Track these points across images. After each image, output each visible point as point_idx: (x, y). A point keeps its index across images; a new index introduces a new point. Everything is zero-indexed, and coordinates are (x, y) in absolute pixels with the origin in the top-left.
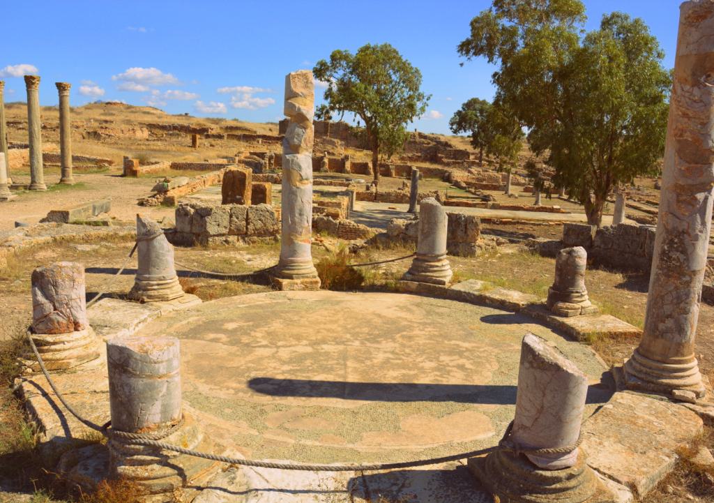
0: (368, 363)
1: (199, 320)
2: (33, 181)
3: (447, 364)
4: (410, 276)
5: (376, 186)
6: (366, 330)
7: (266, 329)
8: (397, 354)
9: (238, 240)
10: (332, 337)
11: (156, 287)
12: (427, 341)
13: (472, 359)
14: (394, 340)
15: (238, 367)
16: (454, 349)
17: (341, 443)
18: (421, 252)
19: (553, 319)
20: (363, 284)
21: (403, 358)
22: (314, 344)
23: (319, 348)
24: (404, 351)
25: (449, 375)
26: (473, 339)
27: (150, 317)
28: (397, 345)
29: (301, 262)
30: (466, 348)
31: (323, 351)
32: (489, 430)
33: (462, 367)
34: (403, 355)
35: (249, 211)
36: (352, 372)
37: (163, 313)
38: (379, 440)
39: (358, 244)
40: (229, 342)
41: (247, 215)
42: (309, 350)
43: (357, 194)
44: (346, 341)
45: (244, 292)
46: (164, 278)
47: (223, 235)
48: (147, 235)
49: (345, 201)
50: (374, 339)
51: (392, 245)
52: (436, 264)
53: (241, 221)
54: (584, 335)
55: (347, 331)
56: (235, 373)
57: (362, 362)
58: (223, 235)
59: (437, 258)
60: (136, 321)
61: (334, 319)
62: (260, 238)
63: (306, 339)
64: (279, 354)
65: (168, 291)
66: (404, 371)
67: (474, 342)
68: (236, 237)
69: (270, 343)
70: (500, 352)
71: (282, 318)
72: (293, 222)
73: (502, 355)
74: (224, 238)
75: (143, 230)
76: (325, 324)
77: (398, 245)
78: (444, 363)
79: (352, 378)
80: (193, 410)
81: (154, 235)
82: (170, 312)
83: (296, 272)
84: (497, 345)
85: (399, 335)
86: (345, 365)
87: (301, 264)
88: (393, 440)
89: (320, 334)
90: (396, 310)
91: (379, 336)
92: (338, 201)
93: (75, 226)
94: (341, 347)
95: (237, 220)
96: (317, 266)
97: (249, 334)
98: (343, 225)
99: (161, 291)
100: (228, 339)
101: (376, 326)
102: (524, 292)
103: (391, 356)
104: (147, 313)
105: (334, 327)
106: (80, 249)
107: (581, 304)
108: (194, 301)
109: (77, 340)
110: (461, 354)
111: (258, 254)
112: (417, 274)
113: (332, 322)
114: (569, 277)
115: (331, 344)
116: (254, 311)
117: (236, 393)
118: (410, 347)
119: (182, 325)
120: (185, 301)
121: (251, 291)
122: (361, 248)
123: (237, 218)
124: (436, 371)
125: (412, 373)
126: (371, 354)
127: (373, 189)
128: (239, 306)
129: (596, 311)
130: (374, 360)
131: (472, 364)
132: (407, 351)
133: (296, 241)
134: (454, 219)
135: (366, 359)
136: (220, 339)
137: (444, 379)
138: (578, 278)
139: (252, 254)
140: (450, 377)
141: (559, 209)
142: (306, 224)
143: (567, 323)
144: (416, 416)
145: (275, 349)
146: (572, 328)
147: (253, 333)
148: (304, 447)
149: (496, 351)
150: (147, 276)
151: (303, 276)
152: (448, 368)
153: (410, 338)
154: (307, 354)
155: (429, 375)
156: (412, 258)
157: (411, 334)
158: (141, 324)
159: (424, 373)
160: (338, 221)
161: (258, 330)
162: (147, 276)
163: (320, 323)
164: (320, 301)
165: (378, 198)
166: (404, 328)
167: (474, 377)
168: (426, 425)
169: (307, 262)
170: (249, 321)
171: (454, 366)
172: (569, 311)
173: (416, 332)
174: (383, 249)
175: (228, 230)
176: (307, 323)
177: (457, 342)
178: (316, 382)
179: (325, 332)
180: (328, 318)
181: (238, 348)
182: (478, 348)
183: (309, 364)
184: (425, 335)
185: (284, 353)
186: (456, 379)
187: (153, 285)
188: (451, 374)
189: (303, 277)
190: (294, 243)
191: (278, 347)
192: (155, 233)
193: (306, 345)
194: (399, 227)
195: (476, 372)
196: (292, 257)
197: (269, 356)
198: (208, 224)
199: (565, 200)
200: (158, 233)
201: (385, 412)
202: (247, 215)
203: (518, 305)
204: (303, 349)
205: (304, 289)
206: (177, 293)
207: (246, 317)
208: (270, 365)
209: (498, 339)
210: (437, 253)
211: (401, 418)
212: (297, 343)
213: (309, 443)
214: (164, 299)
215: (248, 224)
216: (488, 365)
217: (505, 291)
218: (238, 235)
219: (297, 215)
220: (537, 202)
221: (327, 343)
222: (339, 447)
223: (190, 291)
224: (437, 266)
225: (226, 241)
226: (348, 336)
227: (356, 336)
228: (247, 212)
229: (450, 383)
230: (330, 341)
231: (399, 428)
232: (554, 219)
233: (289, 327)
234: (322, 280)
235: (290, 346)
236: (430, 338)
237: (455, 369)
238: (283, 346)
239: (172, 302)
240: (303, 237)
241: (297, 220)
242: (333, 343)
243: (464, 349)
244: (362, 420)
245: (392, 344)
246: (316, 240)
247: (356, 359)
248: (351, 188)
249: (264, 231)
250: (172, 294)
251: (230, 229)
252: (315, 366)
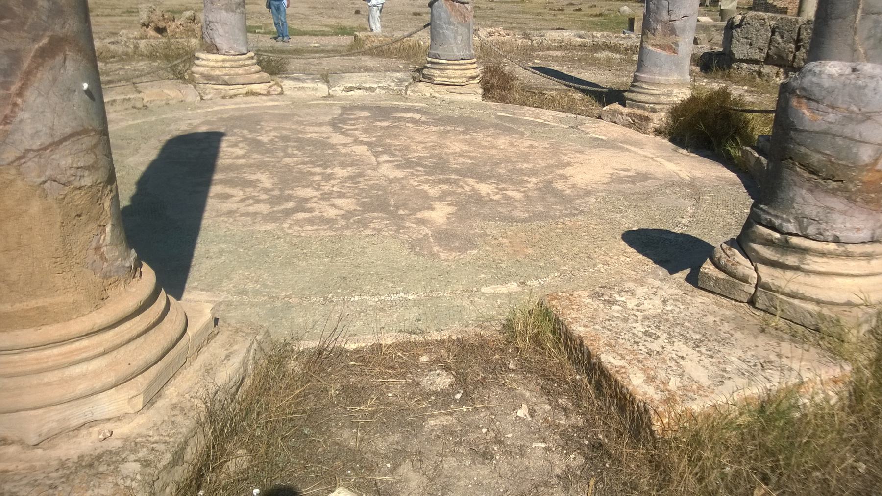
29: (646, 82)
41: (799, 34)
46: (437, 57)
47: (756, 62)
58: (756, 62)
65: (437, 73)
68: (775, 69)
74: (756, 68)
87: (644, 86)
95: (780, 40)
99: (432, 71)
107: (767, 274)
109: (208, 60)
123: (782, 37)
138: (786, 174)
175: (764, 55)
198: (734, 41)
202: (799, 34)
205: (629, 126)
225: (760, 74)
250: (439, 76)
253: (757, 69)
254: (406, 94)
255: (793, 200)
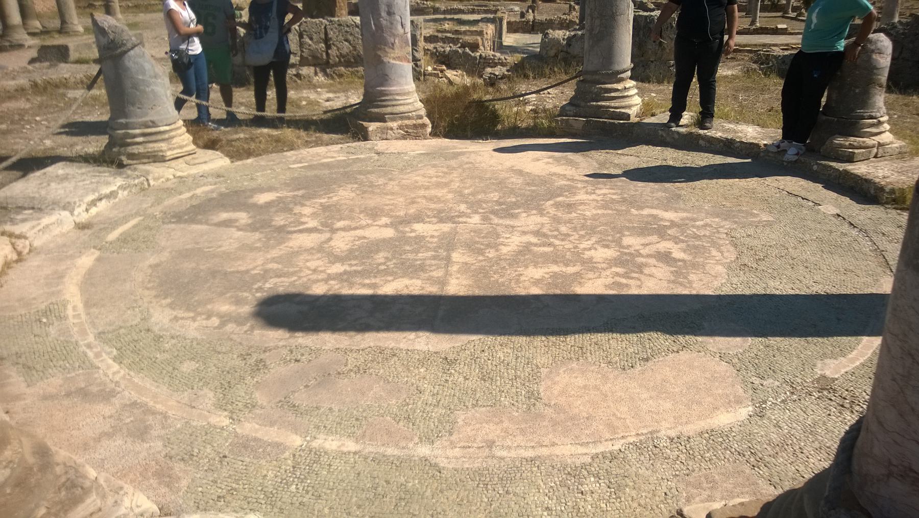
0: (491, 254)
1: (212, 191)
2: (63, 22)
3: (637, 251)
4: (572, 108)
5: (533, 12)
6: (495, 196)
7: (323, 201)
8: (545, 235)
9: (316, 74)
10: (433, 210)
11: (140, 139)
12: (600, 212)
13: (683, 241)
14: (541, 212)
15: (247, 271)
16: (648, 223)
17: (403, 444)
18: (590, 68)
19: (825, 166)
20: (499, 127)
21: (557, 242)
22: (399, 223)
23: (407, 229)
24: (557, 230)
25: (642, 272)
26: (682, 206)
27: (125, 189)
28: (545, 220)
29: (398, 94)
30: (672, 221)
31: (413, 234)
32: (739, 401)
33: (665, 257)
34: (555, 237)
35: (328, 27)
36: (458, 272)
37: (152, 183)
38: (491, 431)
39: (497, 73)
40: (249, 225)
41: (326, 34)
42: (389, 233)
43: (508, 23)
44: (459, 216)
45: (307, 144)
46: (154, 124)
48: (109, 49)
49: (490, 29)
50: (508, 212)
51: (547, 71)
52: (615, 86)
53: (318, 42)
54: (893, 191)
55: (461, 197)
56: (244, 281)
57: (480, 252)
59: (615, 77)
60: (91, 197)
61: (443, 180)
62: (350, 69)
63: (387, 215)
64: (332, 243)
65: (163, 146)
66: (555, 268)
67: (685, 210)
68: (312, 69)
69: (323, 225)
70: (735, 226)
71: (356, 183)
72: (379, 27)
73: (740, 233)
75: (104, 41)
76: (427, 188)
77: (556, 69)
78: (632, 250)
79: (457, 286)
80: (116, 367)
81: (124, 49)
82: (168, 180)
83: (389, 110)
84: (727, 215)
85: (551, 202)
86: (448, 259)
88: (523, 432)
89: (415, 206)
90: (548, 163)
91: (516, 205)
92: (479, 29)
93: (78, 66)
94: (446, 227)
95: (310, 42)
96: (426, 102)
97: (290, 210)
98: (485, 58)
99: (151, 145)
100: (250, 221)
101: (513, 190)
102: (763, 126)
103: (534, 240)
104: (119, 181)
105: (440, 193)
106: (69, 96)
107: (877, 138)
108: (217, 161)
110: (661, 232)
111: (344, 92)
112: (583, 104)
113: (438, 185)
114: (857, 91)
115: (430, 222)
116: (316, 172)
117: (223, 324)
118: (570, 221)
119: (181, 201)
120: (196, 161)
121: (319, 143)
122: (502, 78)
123: (311, 39)
124: (616, 266)
125: (571, 270)
126: (498, 236)
127: (530, 16)
128: (292, 166)
129: (904, 150)
130: (502, 247)
131: (684, 251)
132: (564, 229)
133: (385, 60)
134: (642, 24)
135: (489, 246)
136: (236, 220)
137: (632, 282)
139: (335, 92)
140: (642, 277)
141: (786, 29)
142: (401, 31)
143: (855, 172)
144: (574, 365)
145: (328, 235)
146: (866, 180)
147: (297, 209)
148: (318, 455)
149: (727, 224)
150: (123, 121)
151: (401, 116)
152: (640, 260)
153: (570, 207)
154: (384, 240)
155: (604, 274)
156: (574, 81)
157: (573, 199)
158: (104, 201)
159: (593, 269)
160: (478, 54)
161: (308, 203)
162: (123, 121)
163: (420, 188)
164: (428, 154)
165: (536, 28)
166: (561, 191)
167: (692, 277)
168: (596, 388)
169: (408, 95)
170: (299, 189)
171: (649, 256)
172: (856, 151)
173: (581, 196)
174: (534, 78)
175: (298, 58)
176: (397, 188)
177: (654, 212)
178: (386, 296)
179: (424, 201)
180: (435, 179)
181: (261, 236)
182: (694, 220)
183: (382, 260)
184: (597, 201)
185: (341, 243)
186: (655, 282)
187: (135, 136)
188: (646, 271)
189: (402, 118)
190: (382, 62)
191: (334, 231)
192: (125, 45)
193: (386, 226)
194: (558, 41)
195: (695, 266)
196: (382, 85)
197: (312, 248)
199: (792, 19)
200: (129, 45)
201: (511, 358)
202: (326, 34)
203: (757, 145)
204: (380, 231)
205: (404, 138)
206: (181, 147)
207: (296, 183)
208: (308, 264)
209: (728, 204)
210: (617, 68)
211: (544, 371)
212: (370, 222)
213: (331, 443)
214: (157, 158)
215: (328, 47)
216: (714, 252)
217: (731, 126)
218: (314, 65)
219: (384, 14)
220: (753, 22)
221: (423, 222)
222: (396, 452)
223: (211, 145)
224: (617, 90)
226: (463, 207)
227: (475, 206)
228: (325, 28)
229: (644, 291)
230: (428, 217)
231: (538, 399)
232: (779, 42)
233: (366, 195)
234: (433, 123)
235: (356, 228)
236: (605, 207)
237: (652, 261)
238: (344, 229)
239: (173, 163)
240: (397, 52)
241: (384, 22)
242: (435, 220)
243: (667, 224)
244: (461, 379)
245: (538, 219)
246: (435, 69)
247: (471, 247)
248: (499, 14)
249: (354, 58)
250: (170, 149)
251: (301, 56)
252: (391, 264)
253: (295, 72)
254: (149, 185)
255: (875, 102)
